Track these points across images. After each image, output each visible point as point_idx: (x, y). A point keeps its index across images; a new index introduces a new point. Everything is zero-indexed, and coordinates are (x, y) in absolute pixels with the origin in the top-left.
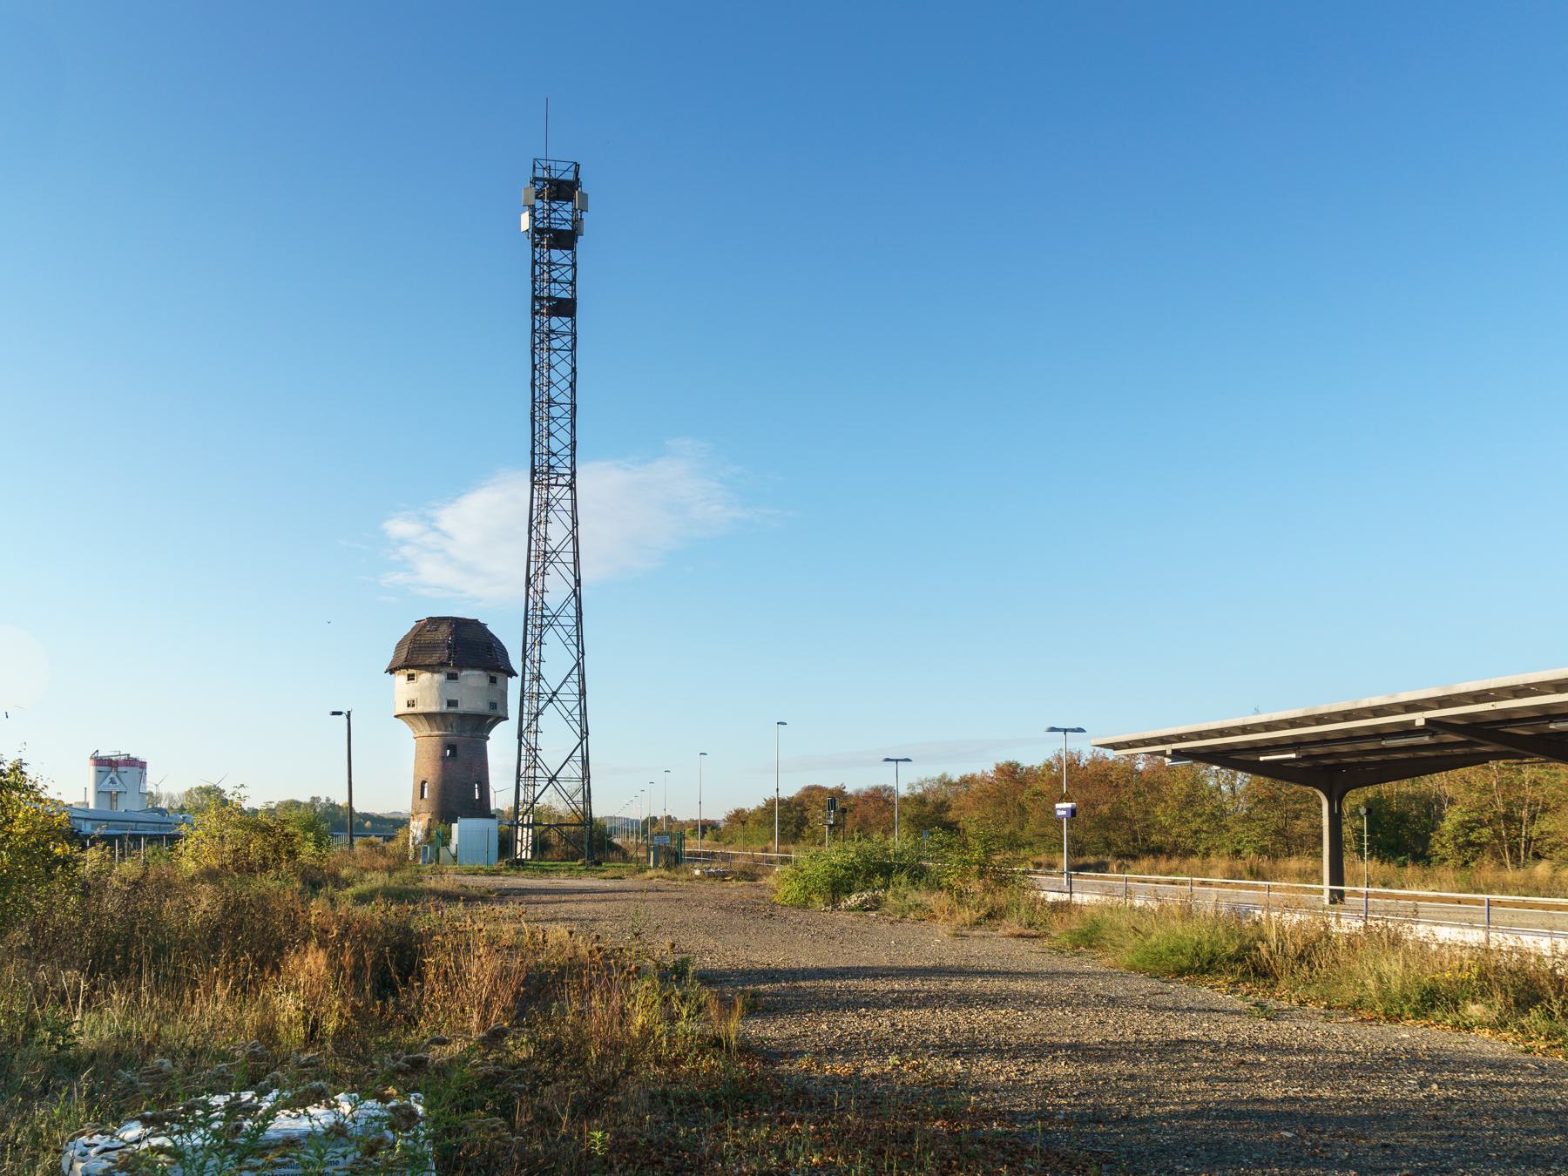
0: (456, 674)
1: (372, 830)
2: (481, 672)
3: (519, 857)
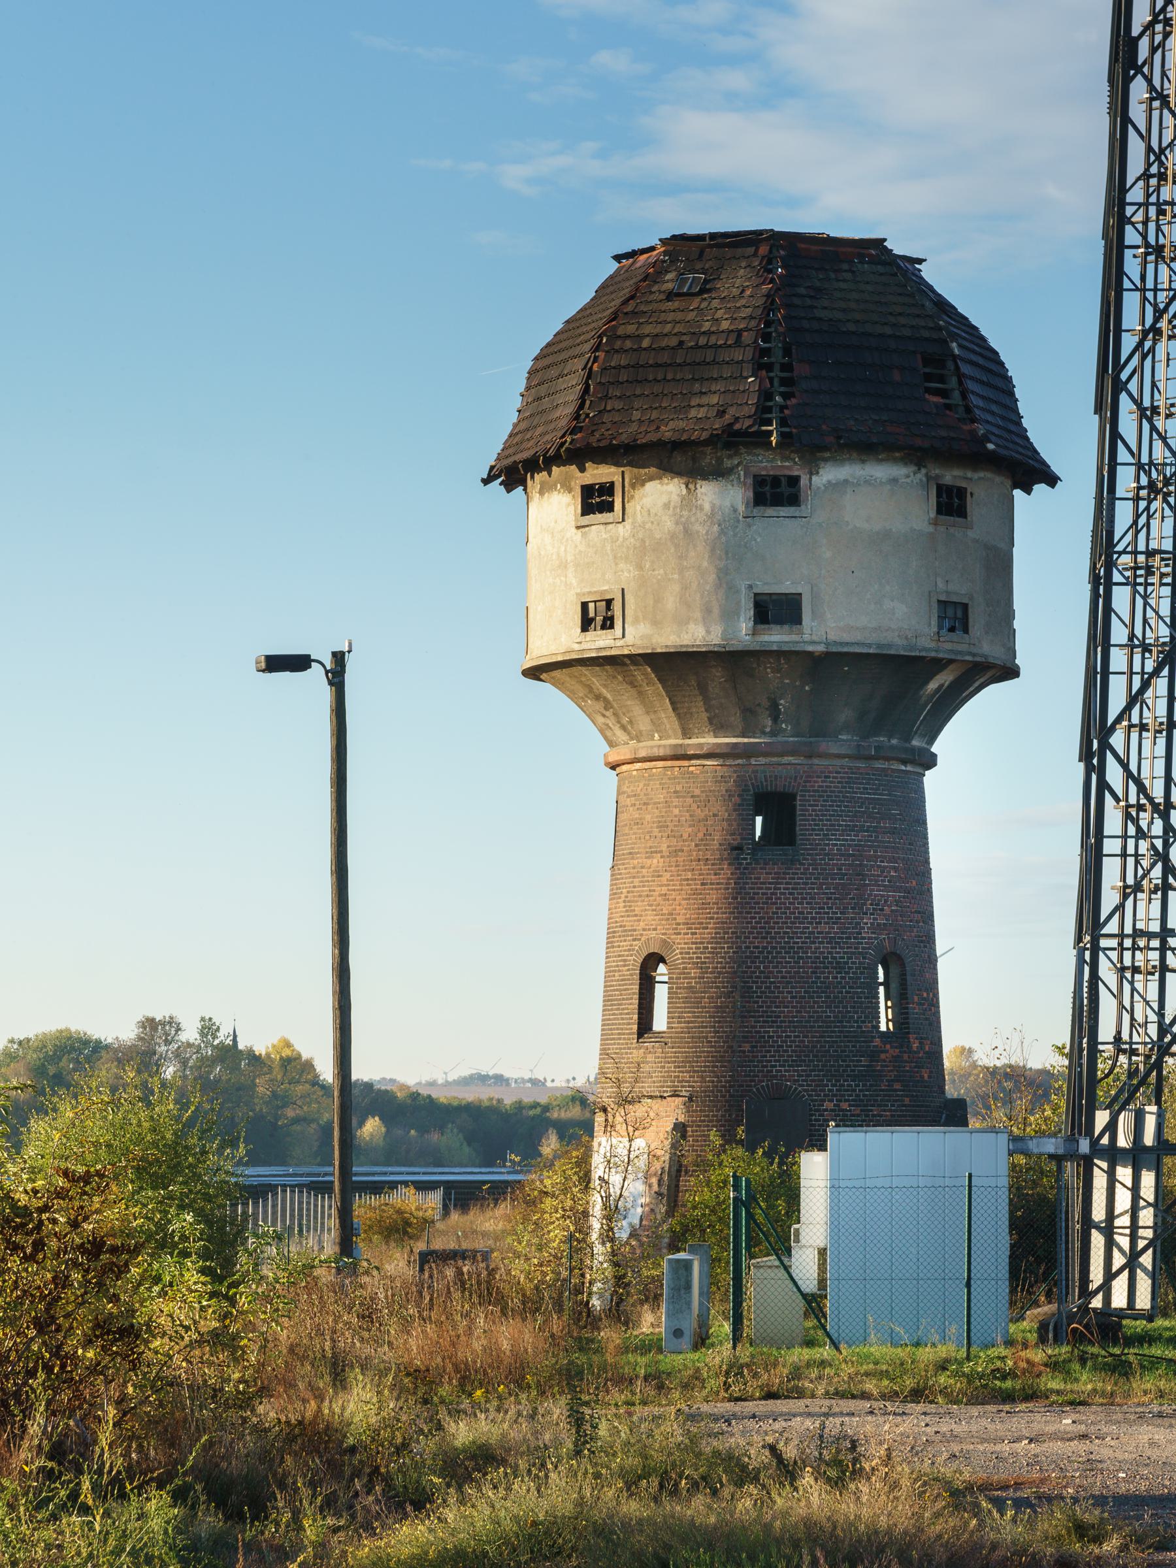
0: (794, 481)
1: (392, 1153)
2: (899, 471)
3: (1097, 1302)
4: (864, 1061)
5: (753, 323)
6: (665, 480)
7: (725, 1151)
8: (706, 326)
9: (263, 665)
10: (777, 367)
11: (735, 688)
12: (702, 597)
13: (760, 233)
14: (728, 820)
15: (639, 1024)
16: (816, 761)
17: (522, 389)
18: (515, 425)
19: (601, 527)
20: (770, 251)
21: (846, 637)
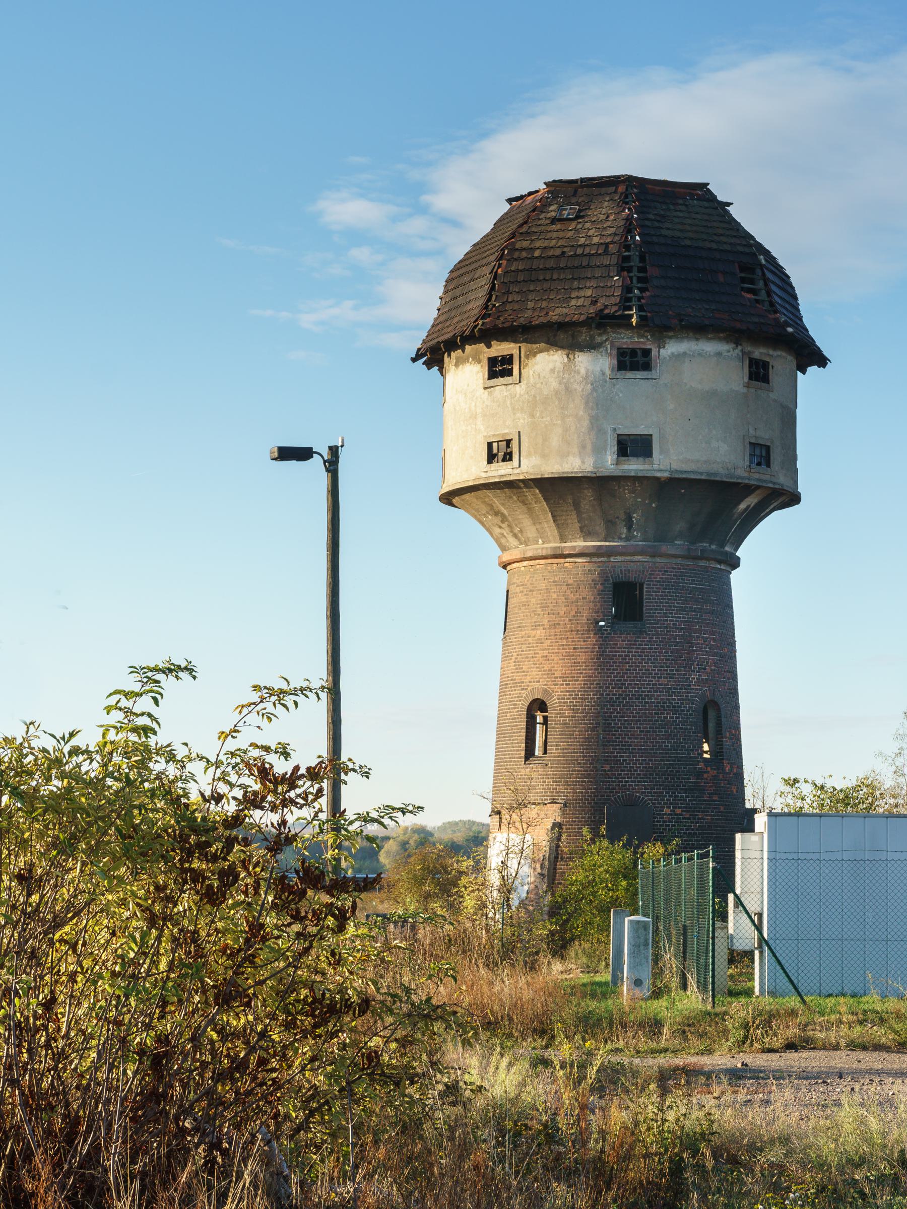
0: (647, 353)
2: (723, 347)
4: (692, 779)
5: (617, 238)
6: (552, 352)
7: (594, 843)
8: (582, 241)
9: (276, 455)
10: (635, 269)
11: (601, 505)
12: (579, 437)
13: (619, 177)
14: (593, 602)
15: (526, 750)
16: (658, 560)
17: (441, 293)
18: (436, 320)
19: (503, 387)
20: (627, 189)
21: (685, 467)
